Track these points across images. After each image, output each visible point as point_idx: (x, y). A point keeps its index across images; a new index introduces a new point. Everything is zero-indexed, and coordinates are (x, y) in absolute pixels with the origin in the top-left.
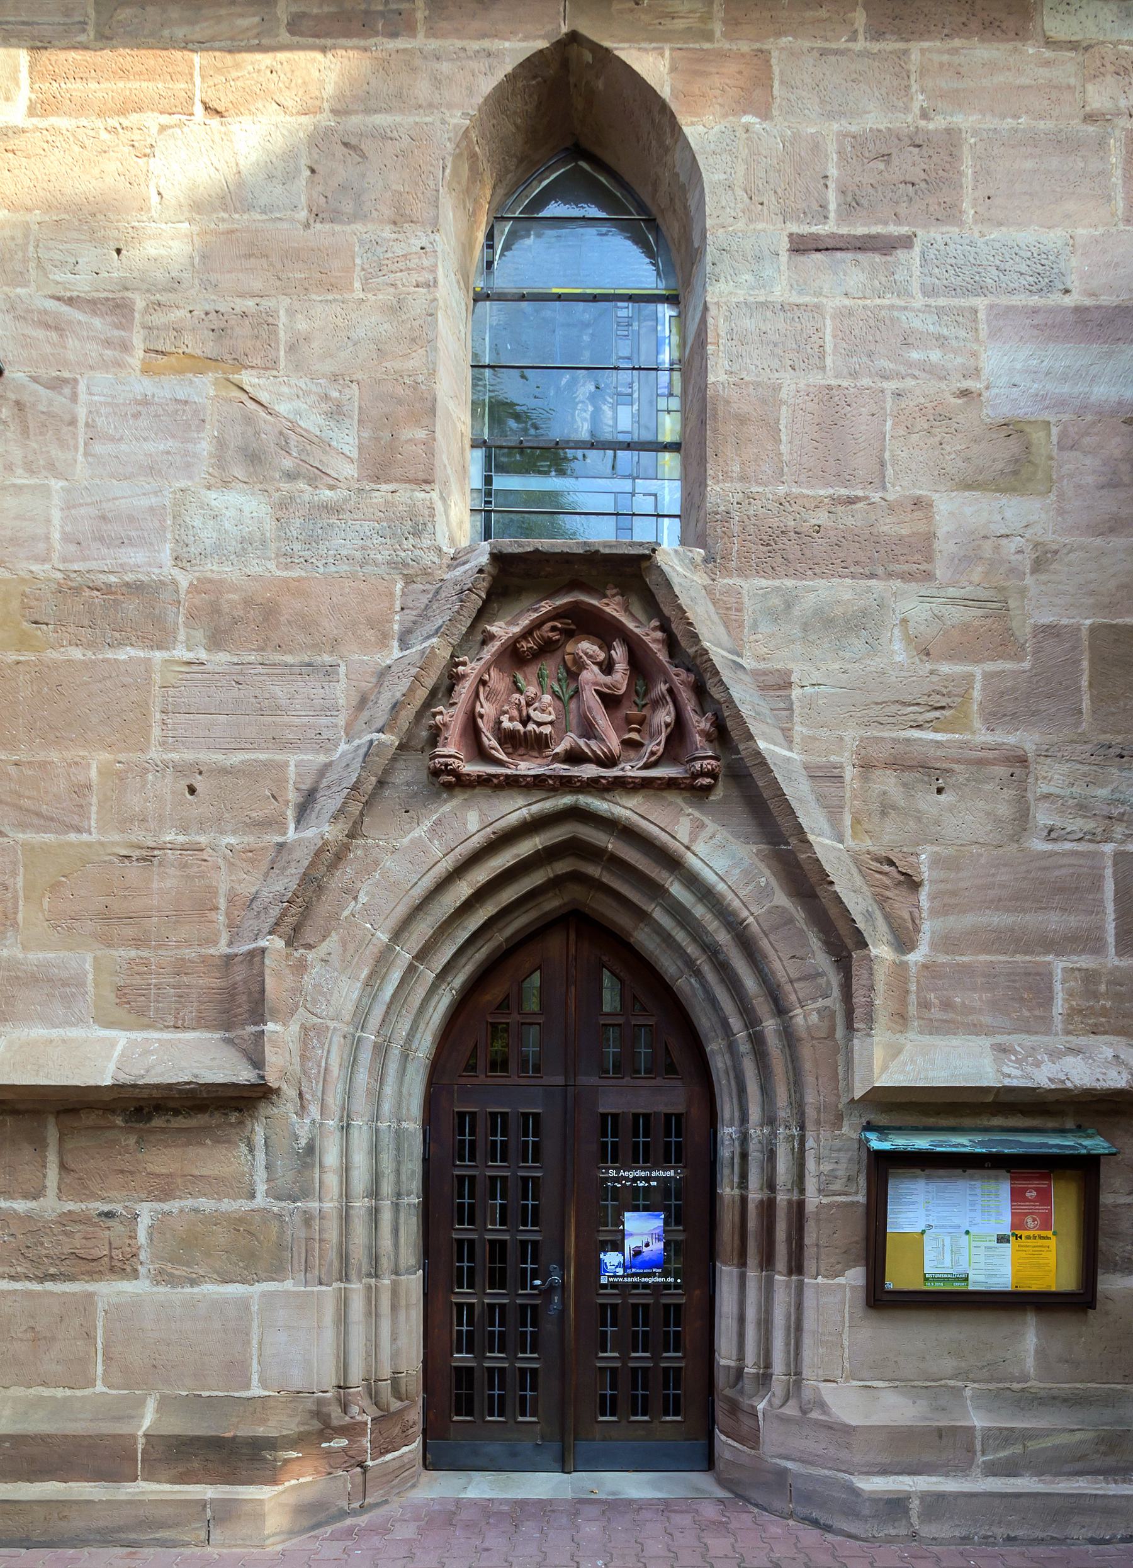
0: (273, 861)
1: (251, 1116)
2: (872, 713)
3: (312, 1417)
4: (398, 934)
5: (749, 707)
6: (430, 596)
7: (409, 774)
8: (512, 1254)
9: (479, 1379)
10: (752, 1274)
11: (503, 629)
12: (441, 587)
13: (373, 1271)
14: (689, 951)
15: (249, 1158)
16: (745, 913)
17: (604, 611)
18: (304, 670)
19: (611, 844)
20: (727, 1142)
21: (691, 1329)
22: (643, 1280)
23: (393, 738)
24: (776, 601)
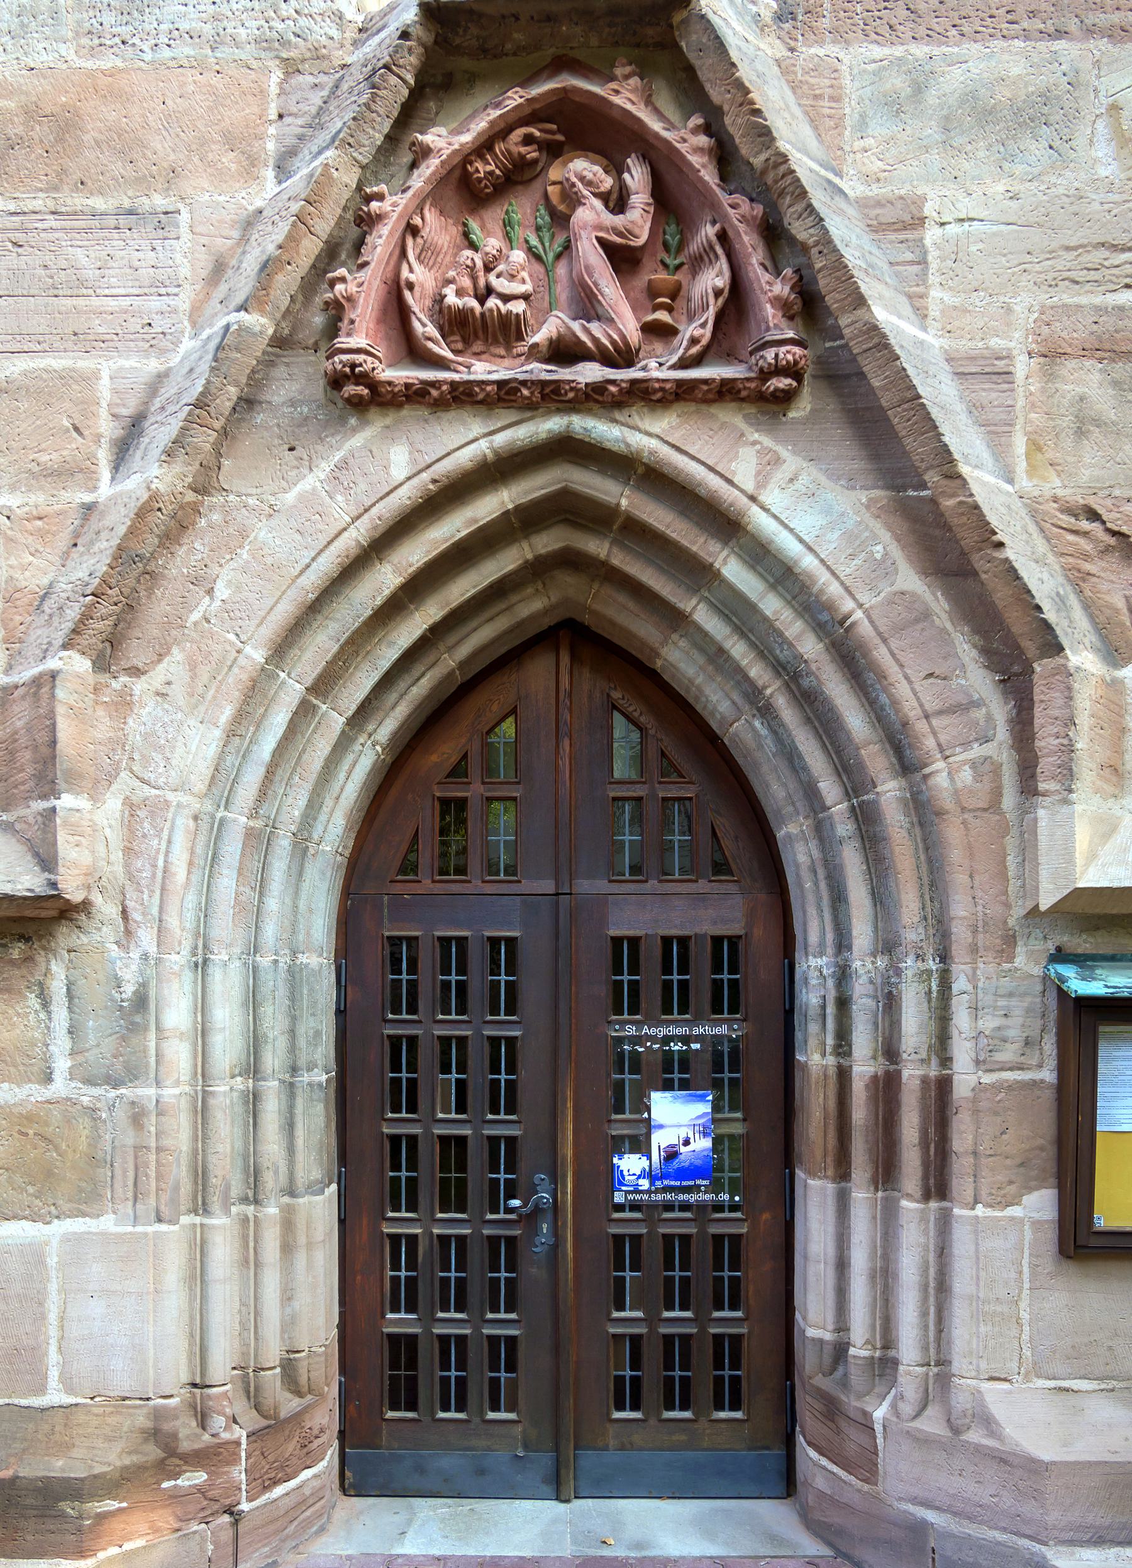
0: (77, 535)
1: (44, 948)
2: (1060, 264)
3: (146, 1440)
4: (283, 647)
5: (857, 254)
6: (325, 93)
7: (296, 385)
8: (476, 1158)
9: (427, 1355)
10: (861, 1195)
11: (444, 139)
12: (343, 77)
13: (251, 1194)
14: (753, 673)
15: (43, 1015)
16: (848, 605)
17: (611, 104)
18: (123, 221)
19: (624, 498)
20: (814, 982)
21: (757, 1276)
22: (681, 1197)
23: (263, 320)
24: (897, 82)
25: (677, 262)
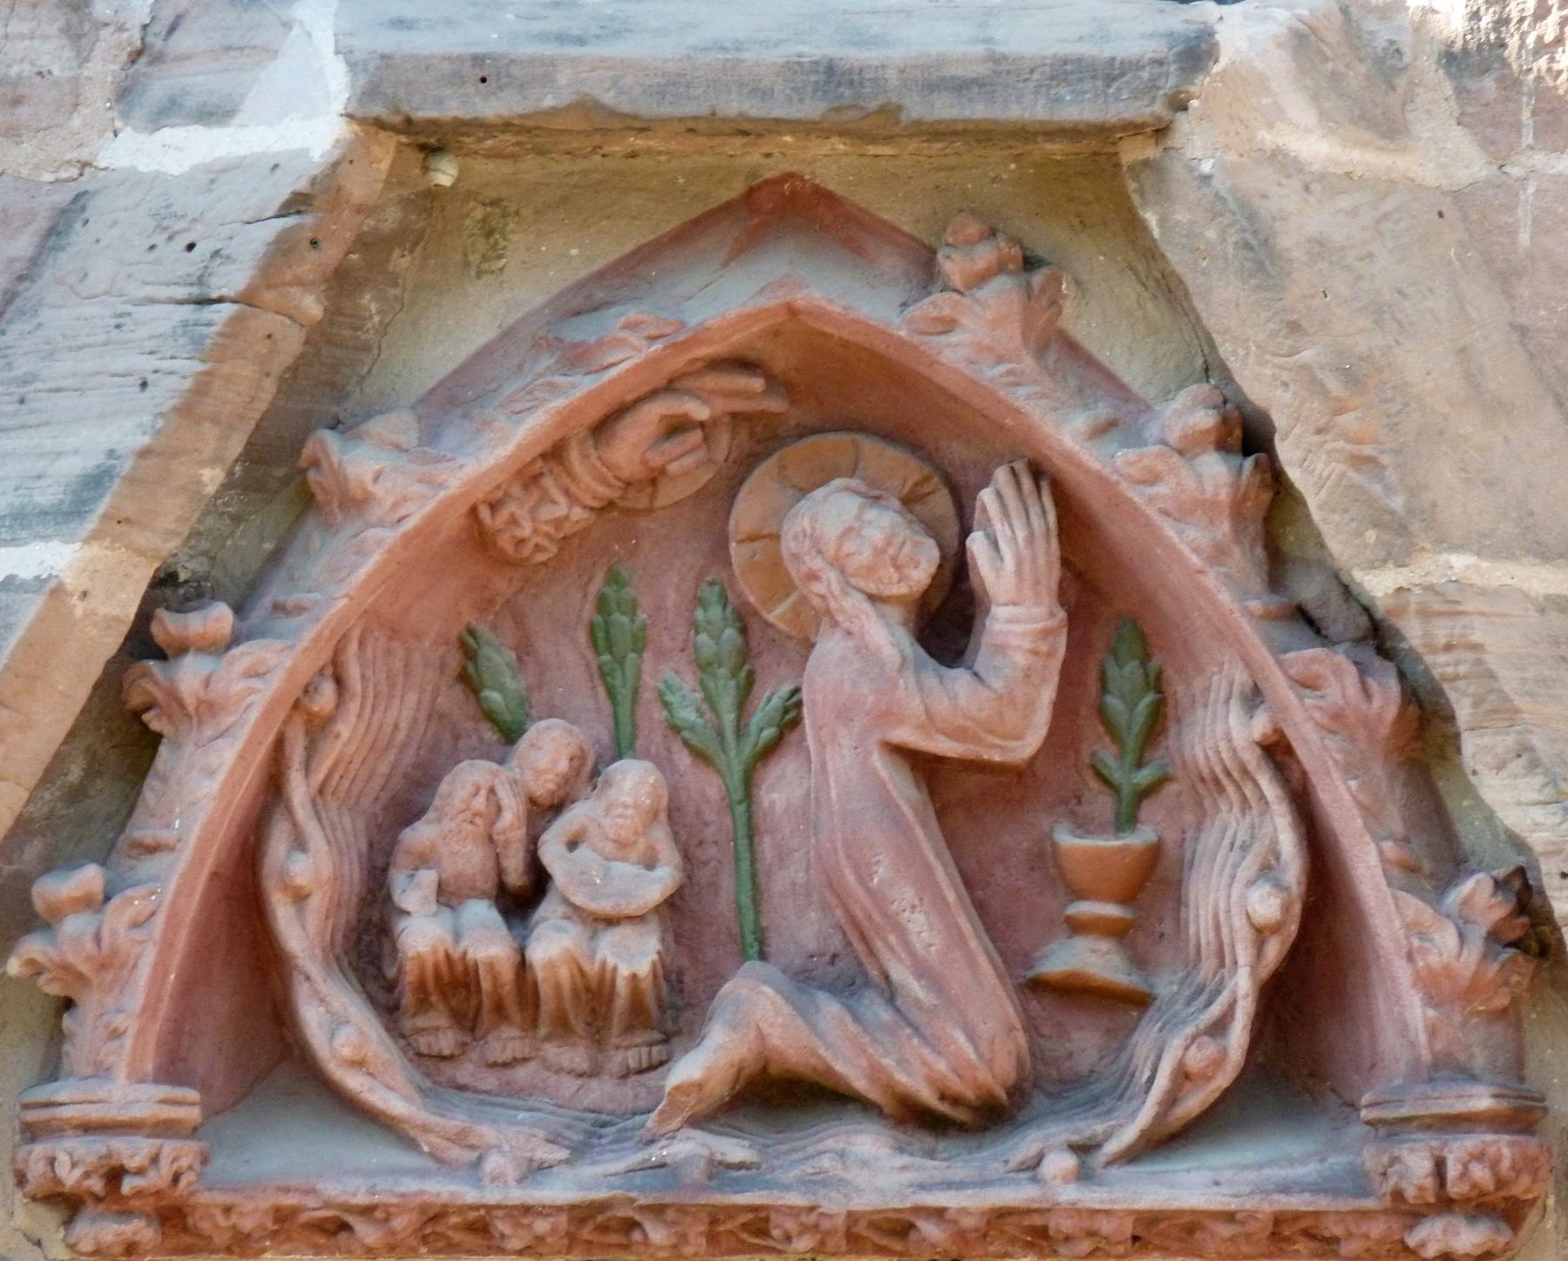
25: (1144, 776)
